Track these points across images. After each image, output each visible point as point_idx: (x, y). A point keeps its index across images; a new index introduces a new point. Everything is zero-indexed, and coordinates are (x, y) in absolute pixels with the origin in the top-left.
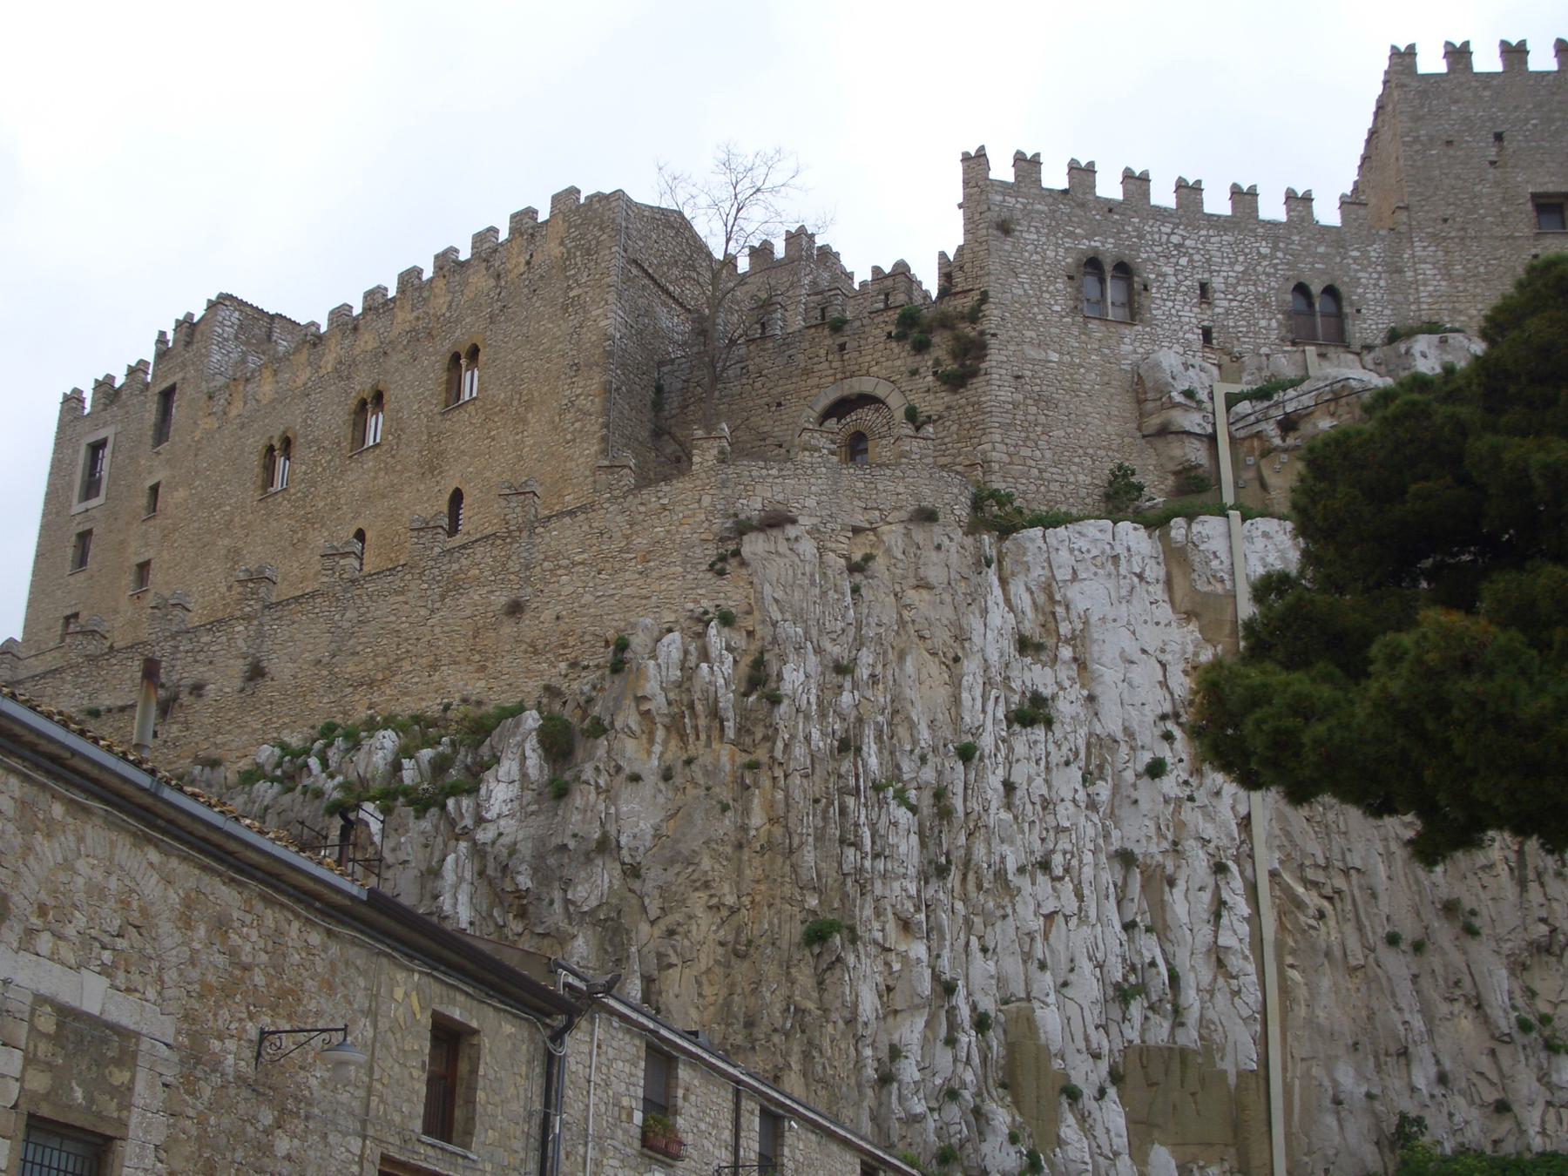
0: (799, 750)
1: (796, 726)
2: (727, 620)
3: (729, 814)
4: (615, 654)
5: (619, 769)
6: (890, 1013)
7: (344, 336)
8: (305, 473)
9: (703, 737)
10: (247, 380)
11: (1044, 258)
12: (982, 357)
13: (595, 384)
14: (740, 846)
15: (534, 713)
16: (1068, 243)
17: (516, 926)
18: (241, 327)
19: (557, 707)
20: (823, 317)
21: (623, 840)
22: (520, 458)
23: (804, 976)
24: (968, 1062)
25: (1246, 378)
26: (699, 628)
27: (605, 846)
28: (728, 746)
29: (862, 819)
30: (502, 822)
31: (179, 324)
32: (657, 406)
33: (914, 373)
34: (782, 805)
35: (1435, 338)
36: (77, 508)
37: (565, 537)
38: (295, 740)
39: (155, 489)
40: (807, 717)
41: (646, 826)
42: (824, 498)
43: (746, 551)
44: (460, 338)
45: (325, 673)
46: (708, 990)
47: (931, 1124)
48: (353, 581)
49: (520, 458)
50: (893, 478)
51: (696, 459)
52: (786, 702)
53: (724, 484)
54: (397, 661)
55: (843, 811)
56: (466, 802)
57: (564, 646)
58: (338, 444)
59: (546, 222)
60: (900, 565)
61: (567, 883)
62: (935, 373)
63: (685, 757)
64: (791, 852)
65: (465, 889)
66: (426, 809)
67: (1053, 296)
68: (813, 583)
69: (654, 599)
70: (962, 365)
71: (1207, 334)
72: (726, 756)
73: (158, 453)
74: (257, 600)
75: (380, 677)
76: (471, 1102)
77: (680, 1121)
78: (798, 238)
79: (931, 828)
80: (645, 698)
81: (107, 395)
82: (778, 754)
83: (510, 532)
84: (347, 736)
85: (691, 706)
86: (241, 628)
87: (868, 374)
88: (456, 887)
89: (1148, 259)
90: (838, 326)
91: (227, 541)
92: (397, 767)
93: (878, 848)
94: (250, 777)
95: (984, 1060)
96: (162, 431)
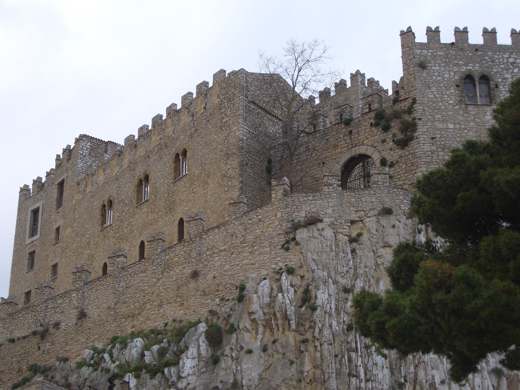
0: (326, 332)
1: (325, 321)
2: (290, 271)
3: (294, 365)
4: (240, 293)
5: (242, 348)
7: (131, 151)
8: (119, 217)
9: (281, 329)
10: (93, 175)
11: (443, 78)
12: (414, 130)
15: (204, 324)
16: (456, 69)
18: (92, 149)
19: (215, 320)
20: (341, 119)
21: (244, 382)
22: (206, 201)
26: (278, 277)
28: (292, 333)
29: (359, 363)
30: (189, 378)
31: (64, 151)
32: (269, 170)
33: (384, 141)
34: (319, 359)
36: (28, 241)
37: (216, 238)
38: (99, 346)
39: (58, 229)
40: (330, 315)
42: (336, 208)
43: (298, 237)
44: (178, 147)
45: (112, 313)
48: (122, 268)
49: (206, 201)
50: (370, 195)
51: (273, 196)
52: (319, 309)
53: (287, 206)
54: (143, 304)
55: (350, 360)
56: (173, 369)
57: (217, 291)
58: (131, 201)
59: (212, 87)
60: (375, 237)
62: (393, 141)
63: (272, 340)
64: (325, 382)
66: (155, 374)
67: (449, 96)
68: (331, 250)
69: (257, 264)
70: (405, 136)
72: (291, 338)
73: (58, 212)
74: (81, 281)
75: (137, 312)
78: (357, 76)
79: (396, 365)
80: (253, 313)
81: (39, 187)
82: (316, 335)
83: (191, 239)
84: (121, 343)
85: (275, 315)
86: (75, 295)
87: (363, 144)
89: (498, 72)
90: (348, 123)
91: (88, 251)
92: (143, 355)
93: (368, 377)
94: (80, 365)
96: (59, 202)
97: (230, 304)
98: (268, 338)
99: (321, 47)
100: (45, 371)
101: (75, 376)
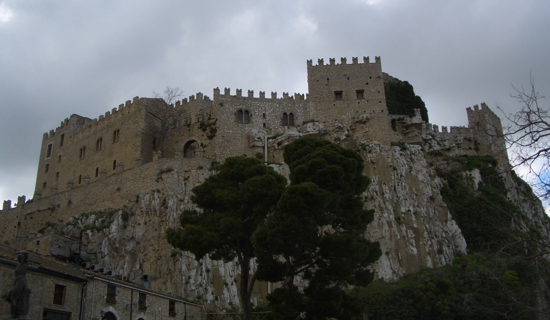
0: (171, 218)
2: (159, 191)
6: (189, 269)
12: (216, 133)
13: (140, 139)
14: (159, 238)
17: (116, 254)
23: (171, 263)
24: (204, 279)
25: (272, 134)
27: (133, 238)
31: (65, 120)
32: (154, 143)
33: (203, 136)
35: (312, 123)
36: (46, 159)
38: (77, 216)
39: (60, 156)
41: (141, 234)
43: (162, 177)
46: (152, 266)
47: (196, 291)
56: (107, 229)
61: (126, 246)
65: (106, 247)
71: (264, 125)
72: (156, 219)
76: (65, 298)
77: (117, 297)
84: (86, 216)
88: (105, 247)
92: (95, 222)
94: (68, 224)
95: (208, 278)
96: (62, 144)
97: (132, 203)
98: (147, 219)
99: (180, 91)
100: (53, 225)
101: (66, 229)
